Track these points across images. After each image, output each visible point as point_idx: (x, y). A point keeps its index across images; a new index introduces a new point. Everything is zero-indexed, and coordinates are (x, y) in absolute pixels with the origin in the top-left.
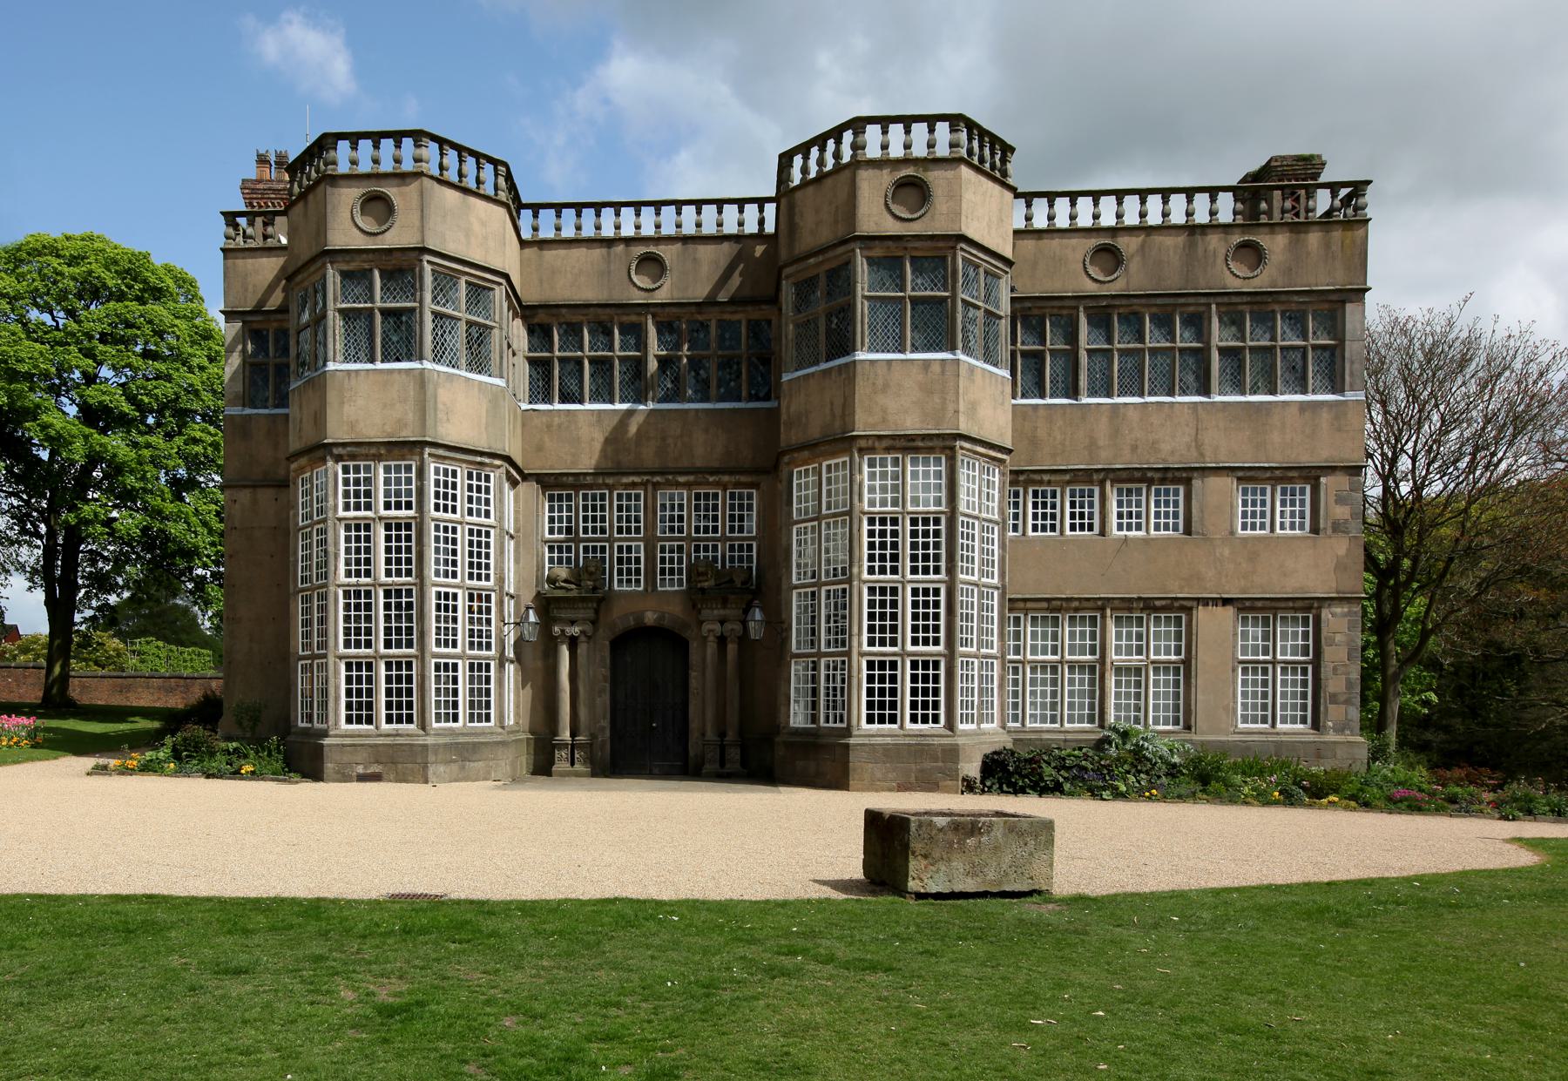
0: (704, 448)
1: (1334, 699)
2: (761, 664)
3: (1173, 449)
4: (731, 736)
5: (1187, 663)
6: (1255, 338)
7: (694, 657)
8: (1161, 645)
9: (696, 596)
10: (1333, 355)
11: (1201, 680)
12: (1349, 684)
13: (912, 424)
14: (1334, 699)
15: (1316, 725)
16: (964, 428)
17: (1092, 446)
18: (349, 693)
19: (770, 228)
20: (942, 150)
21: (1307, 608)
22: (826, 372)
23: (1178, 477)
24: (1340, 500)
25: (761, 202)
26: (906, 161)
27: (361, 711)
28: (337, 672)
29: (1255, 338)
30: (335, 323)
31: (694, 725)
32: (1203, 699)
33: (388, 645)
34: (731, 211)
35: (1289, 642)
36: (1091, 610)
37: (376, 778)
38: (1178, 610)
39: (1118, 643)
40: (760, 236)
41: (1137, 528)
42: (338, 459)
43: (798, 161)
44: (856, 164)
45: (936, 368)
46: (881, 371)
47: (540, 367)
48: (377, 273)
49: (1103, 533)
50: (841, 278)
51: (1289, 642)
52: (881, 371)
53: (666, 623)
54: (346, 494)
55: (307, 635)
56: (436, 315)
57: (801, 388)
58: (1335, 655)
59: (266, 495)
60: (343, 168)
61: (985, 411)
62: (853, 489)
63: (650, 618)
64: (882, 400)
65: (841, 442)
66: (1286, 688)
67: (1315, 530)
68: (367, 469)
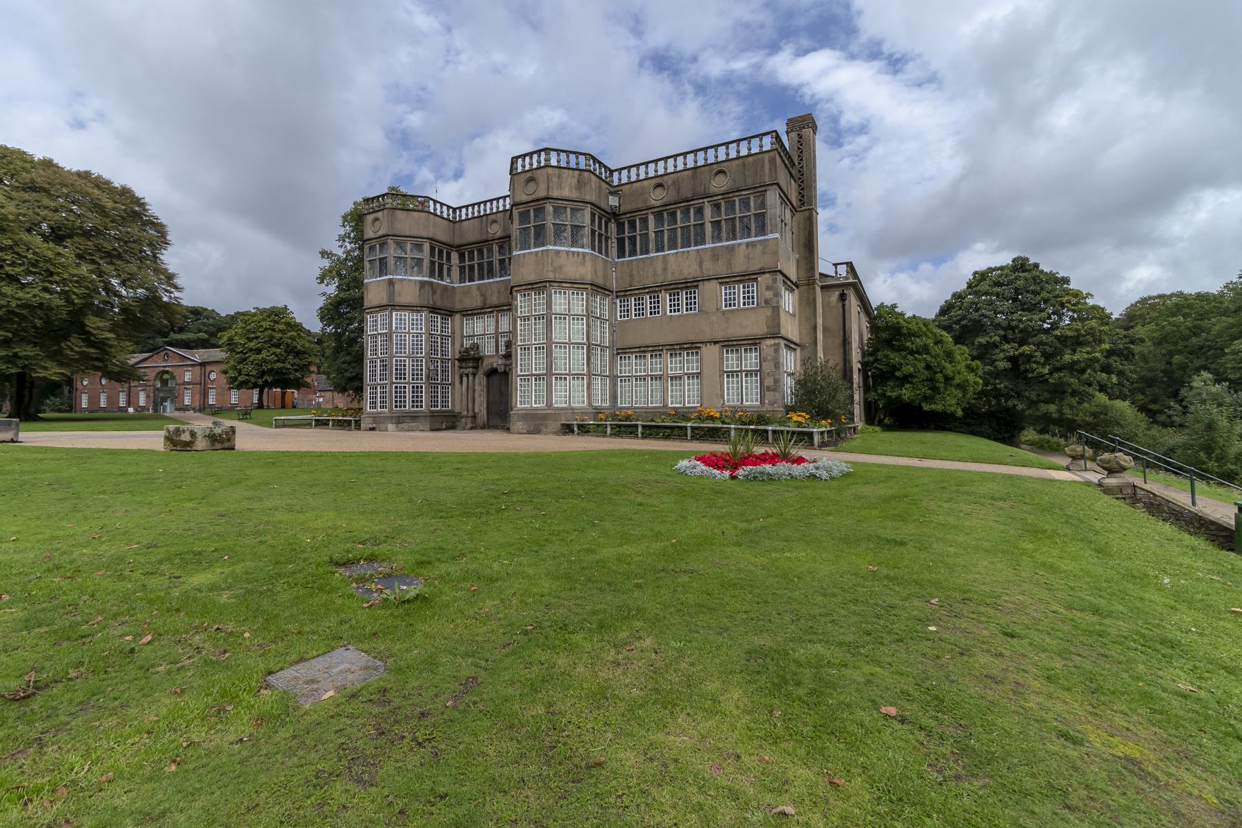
3: (690, 270)
13: (532, 278)
17: (655, 274)
23: (691, 285)
37: (373, 429)
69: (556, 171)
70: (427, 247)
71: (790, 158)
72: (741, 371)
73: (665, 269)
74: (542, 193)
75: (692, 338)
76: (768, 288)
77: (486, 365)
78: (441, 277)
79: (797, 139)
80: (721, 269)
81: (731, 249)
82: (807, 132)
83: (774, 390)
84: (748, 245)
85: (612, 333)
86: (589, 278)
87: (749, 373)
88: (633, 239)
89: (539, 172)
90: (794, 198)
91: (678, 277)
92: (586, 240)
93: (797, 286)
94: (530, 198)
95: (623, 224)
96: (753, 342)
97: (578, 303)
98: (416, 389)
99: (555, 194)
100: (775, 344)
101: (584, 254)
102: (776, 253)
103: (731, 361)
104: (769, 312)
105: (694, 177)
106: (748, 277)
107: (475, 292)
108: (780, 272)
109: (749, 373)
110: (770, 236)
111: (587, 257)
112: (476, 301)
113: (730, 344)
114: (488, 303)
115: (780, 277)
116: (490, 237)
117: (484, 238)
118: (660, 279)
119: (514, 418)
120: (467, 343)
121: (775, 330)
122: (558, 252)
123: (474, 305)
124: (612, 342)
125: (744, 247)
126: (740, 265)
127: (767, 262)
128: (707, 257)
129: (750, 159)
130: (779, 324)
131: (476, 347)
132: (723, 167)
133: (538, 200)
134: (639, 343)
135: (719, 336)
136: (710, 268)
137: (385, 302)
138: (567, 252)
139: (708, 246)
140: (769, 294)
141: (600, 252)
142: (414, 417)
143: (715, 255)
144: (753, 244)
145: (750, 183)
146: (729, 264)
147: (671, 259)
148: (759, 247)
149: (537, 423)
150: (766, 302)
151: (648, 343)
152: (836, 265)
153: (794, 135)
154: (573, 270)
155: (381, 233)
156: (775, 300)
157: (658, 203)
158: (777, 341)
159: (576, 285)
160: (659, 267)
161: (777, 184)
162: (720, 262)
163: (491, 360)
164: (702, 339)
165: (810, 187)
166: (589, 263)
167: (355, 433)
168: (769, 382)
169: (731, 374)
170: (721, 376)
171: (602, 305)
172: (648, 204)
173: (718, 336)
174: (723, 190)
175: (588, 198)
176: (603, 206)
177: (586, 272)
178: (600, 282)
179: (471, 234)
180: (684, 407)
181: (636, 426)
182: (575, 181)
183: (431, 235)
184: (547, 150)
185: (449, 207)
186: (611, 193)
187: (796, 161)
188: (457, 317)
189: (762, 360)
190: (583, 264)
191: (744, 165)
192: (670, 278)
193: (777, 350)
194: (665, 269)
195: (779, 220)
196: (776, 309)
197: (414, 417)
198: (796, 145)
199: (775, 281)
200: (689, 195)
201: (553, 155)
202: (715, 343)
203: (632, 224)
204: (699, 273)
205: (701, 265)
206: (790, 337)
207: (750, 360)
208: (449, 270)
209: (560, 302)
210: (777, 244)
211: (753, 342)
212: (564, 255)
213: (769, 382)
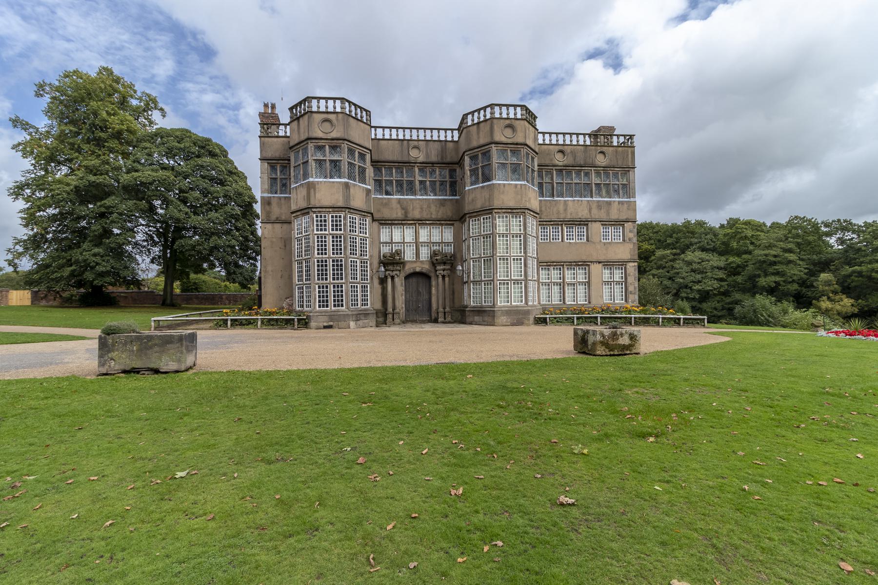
0: (435, 212)
1: (631, 293)
2: (457, 283)
3: (583, 214)
4: (390, 316)
5: (589, 282)
6: (329, 156)
7: (434, 283)
8: (581, 276)
9: (434, 264)
10: (452, 172)
11: (593, 287)
12: (635, 288)
13: (512, 204)
14: (631, 293)
15: (626, 301)
16: (528, 206)
17: (558, 213)
18: (319, 297)
19: (456, 139)
20: (519, 116)
21: (622, 264)
22: (483, 187)
23: (583, 223)
24: (631, 231)
25: (452, 130)
26: (508, 119)
27: (324, 303)
28: (315, 289)
29: (329, 156)
30: (312, 165)
31: (434, 306)
32: (593, 293)
33: (334, 279)
34: (442, 133)
35: (618, 275)
36: (560, 265)
37: (330, 327)
38: (584, 264)
39: (569, 275)
40: (452, 141)
41: (573, 236)
42: (314, 212)
43: (470, 117)
44: (492, 118)
45: (519, 187)
46: (502, 187)
47: (378, 183)
48: (327, 147)
49: (562, 241)
50: (487, 155)
51: (618, 275)
52: (502, 187)
53: (424, 271)
54: (317, 225)
55: (300, 276)
56: (349, 163)
57: (473, 191)
58: (631, 279)
59: (285, 226)
60: (315, 109)
61: (533, 201)
62: (494, 226)
63: (418, 269)
64: (502, 196)
65: (488, 211)
66: (617, 289)
67: (624, 240)
68: (325, 216)
73: (565, 210)
74: (520, 139)
75: (584, 258)
77: (408, 269)
80: (603, 215)
81: (609, 203)
84: (619, 202)
89: (518, 122)
91: (574, 216)
94: (509, 141)
98: (364, 288)
105: (585, 151)
107: (395, 205)
112: (399, 214)
114: (410, 216)
116: (412, 160)
117: (406, 159)
118: (562, 216)
119: (498, 314)
120: (385, 250)
123: (394, 216)
126: (614, 215)
128: (594, 206)
131: (398, 253)
132: (332, 117)
133: (517, 144)
134: (547, 259)
136: (596, 214)
137: (340, 204)
142: (365, 314)
143: (599, 205)
145: (620, 163)
146: (608, 213)
147: (570, 204)
148: (625, 205)
149: (518, 317)
151: (553, 260)
155: (334, 135)
157: (561, 164)
160: (561, 207)
163: (414, 265)
167: (304, 332)
174: (604, 164)
179: (391, 153)
180: (577, 304)
181: (227, 320)
184: (492, 106)
192: (569, 217)
194: (565, 210)
197: (365, 314)
200: (582, 163)
201: (497, 109)
204: (589, 216)
209: (500, 225)
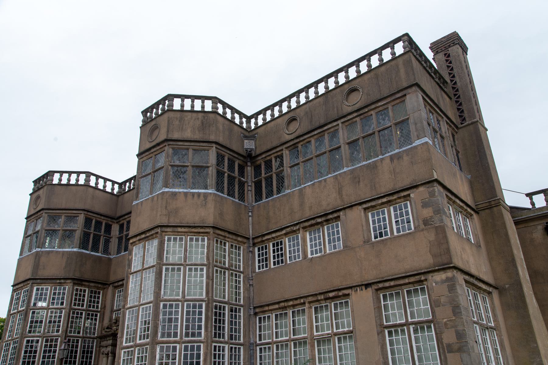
3: (329, 200)
69: (178, 115)
70: (81, 218)
71: (441, 77)
72: (407, 324)
73: (302, 204)
76: (425, 205)
78: (95, 248)
79: (444, 58)
80: (365, 193)
81: (373, 167)
82: (455, 50)
83: (460, 350)
84: (392, 158)
85: (249, 286)
86: (210, 221)
87: (420, 326)
88: (269, 180)
90: (452, 113)
92: (212, 179)
93: (477, 212)
95: (259, 166)
96: (416, 280)
97: (199, 249)
99: (176, 135)
100: (448, 279)
101: (206, 195)
102: (429, 159)
103: (395, 312)
104: (431, 236)
106: (397, 195)
108: (436, 181)
109: (420, 326)
110: (417, 143)
111: (210, 198)
113: (386, 286)
115: (437, 188)
118: (297, 218)
121: (445, 259)
122: (174, 194)
124: (248, 299)
125: (388, 161)
126: (386, 184)
127: (419, 173)
129: (383, 68)
130: (448, 251)
135: (371, 276)
136: (351, 194)
138: (186, 194)
139: (345, 169)
140: (427, 212)
141: (231, 193)
143: (355, 178)
144: (398, 156)
147: (308, 191)
148: (406, 158)
150: (426, 222)
152: (530, 195)
153: (441, 56)
154: (191, 214)
156: (436, 218)
158: (449, 274)
159: (195, 229)
161: (417, 85)
162: (362, 185)
164: (349, 283)
165: (470, 101)
166: (211, 205)
168: (449, 337)
169: (394, 329)
170: (381, 333)
171: (227, 254)
172: (283, 140)
173: (370, 277)
175: (212, 138)
176: (234, 148)
177: (208, 214)
178: (230, 226)
182: (198, 123)
183: (87, 207)
185: (114, 183)
186: (246, 137)
187: (447, 79)
188: (111, 288)
189: (435, 304)
190: (205, 205)
191: (377, 76)
192: (308, 214)
193: (452, 288)
194: (302, 204)
195: (425, 123)
196: (441, 232)
198: (445, 65)
199: (432, 194)
200: (322, 122)
202: (367, 286)
203: (268, 164)
205: (340, 192)
206: (473, 271)
207: (421, 305)
208: (107, 242)
209: (175, 250)
210: (429, 151)
211: (416, 280)
212: (182, 197)
213: (449, 337)
